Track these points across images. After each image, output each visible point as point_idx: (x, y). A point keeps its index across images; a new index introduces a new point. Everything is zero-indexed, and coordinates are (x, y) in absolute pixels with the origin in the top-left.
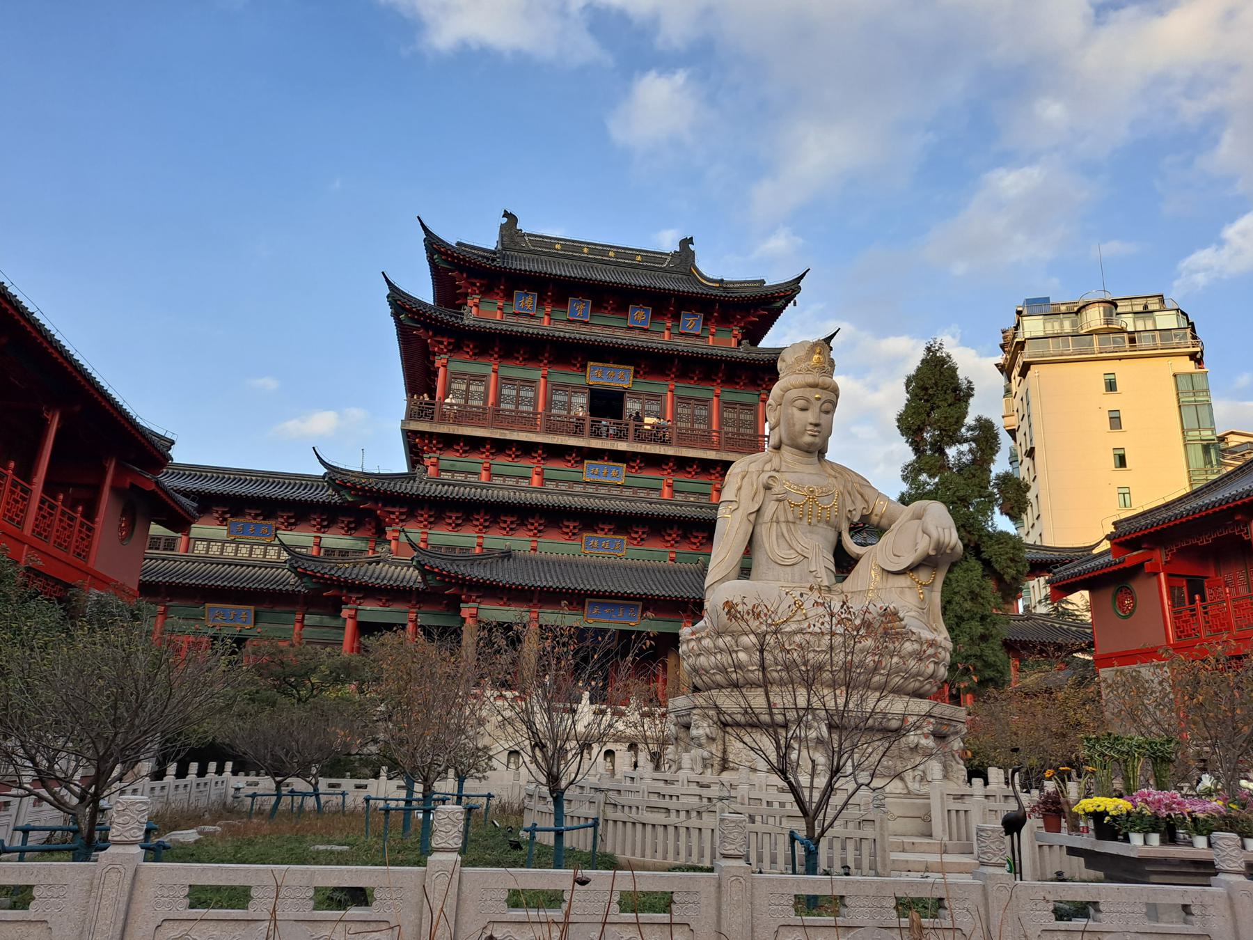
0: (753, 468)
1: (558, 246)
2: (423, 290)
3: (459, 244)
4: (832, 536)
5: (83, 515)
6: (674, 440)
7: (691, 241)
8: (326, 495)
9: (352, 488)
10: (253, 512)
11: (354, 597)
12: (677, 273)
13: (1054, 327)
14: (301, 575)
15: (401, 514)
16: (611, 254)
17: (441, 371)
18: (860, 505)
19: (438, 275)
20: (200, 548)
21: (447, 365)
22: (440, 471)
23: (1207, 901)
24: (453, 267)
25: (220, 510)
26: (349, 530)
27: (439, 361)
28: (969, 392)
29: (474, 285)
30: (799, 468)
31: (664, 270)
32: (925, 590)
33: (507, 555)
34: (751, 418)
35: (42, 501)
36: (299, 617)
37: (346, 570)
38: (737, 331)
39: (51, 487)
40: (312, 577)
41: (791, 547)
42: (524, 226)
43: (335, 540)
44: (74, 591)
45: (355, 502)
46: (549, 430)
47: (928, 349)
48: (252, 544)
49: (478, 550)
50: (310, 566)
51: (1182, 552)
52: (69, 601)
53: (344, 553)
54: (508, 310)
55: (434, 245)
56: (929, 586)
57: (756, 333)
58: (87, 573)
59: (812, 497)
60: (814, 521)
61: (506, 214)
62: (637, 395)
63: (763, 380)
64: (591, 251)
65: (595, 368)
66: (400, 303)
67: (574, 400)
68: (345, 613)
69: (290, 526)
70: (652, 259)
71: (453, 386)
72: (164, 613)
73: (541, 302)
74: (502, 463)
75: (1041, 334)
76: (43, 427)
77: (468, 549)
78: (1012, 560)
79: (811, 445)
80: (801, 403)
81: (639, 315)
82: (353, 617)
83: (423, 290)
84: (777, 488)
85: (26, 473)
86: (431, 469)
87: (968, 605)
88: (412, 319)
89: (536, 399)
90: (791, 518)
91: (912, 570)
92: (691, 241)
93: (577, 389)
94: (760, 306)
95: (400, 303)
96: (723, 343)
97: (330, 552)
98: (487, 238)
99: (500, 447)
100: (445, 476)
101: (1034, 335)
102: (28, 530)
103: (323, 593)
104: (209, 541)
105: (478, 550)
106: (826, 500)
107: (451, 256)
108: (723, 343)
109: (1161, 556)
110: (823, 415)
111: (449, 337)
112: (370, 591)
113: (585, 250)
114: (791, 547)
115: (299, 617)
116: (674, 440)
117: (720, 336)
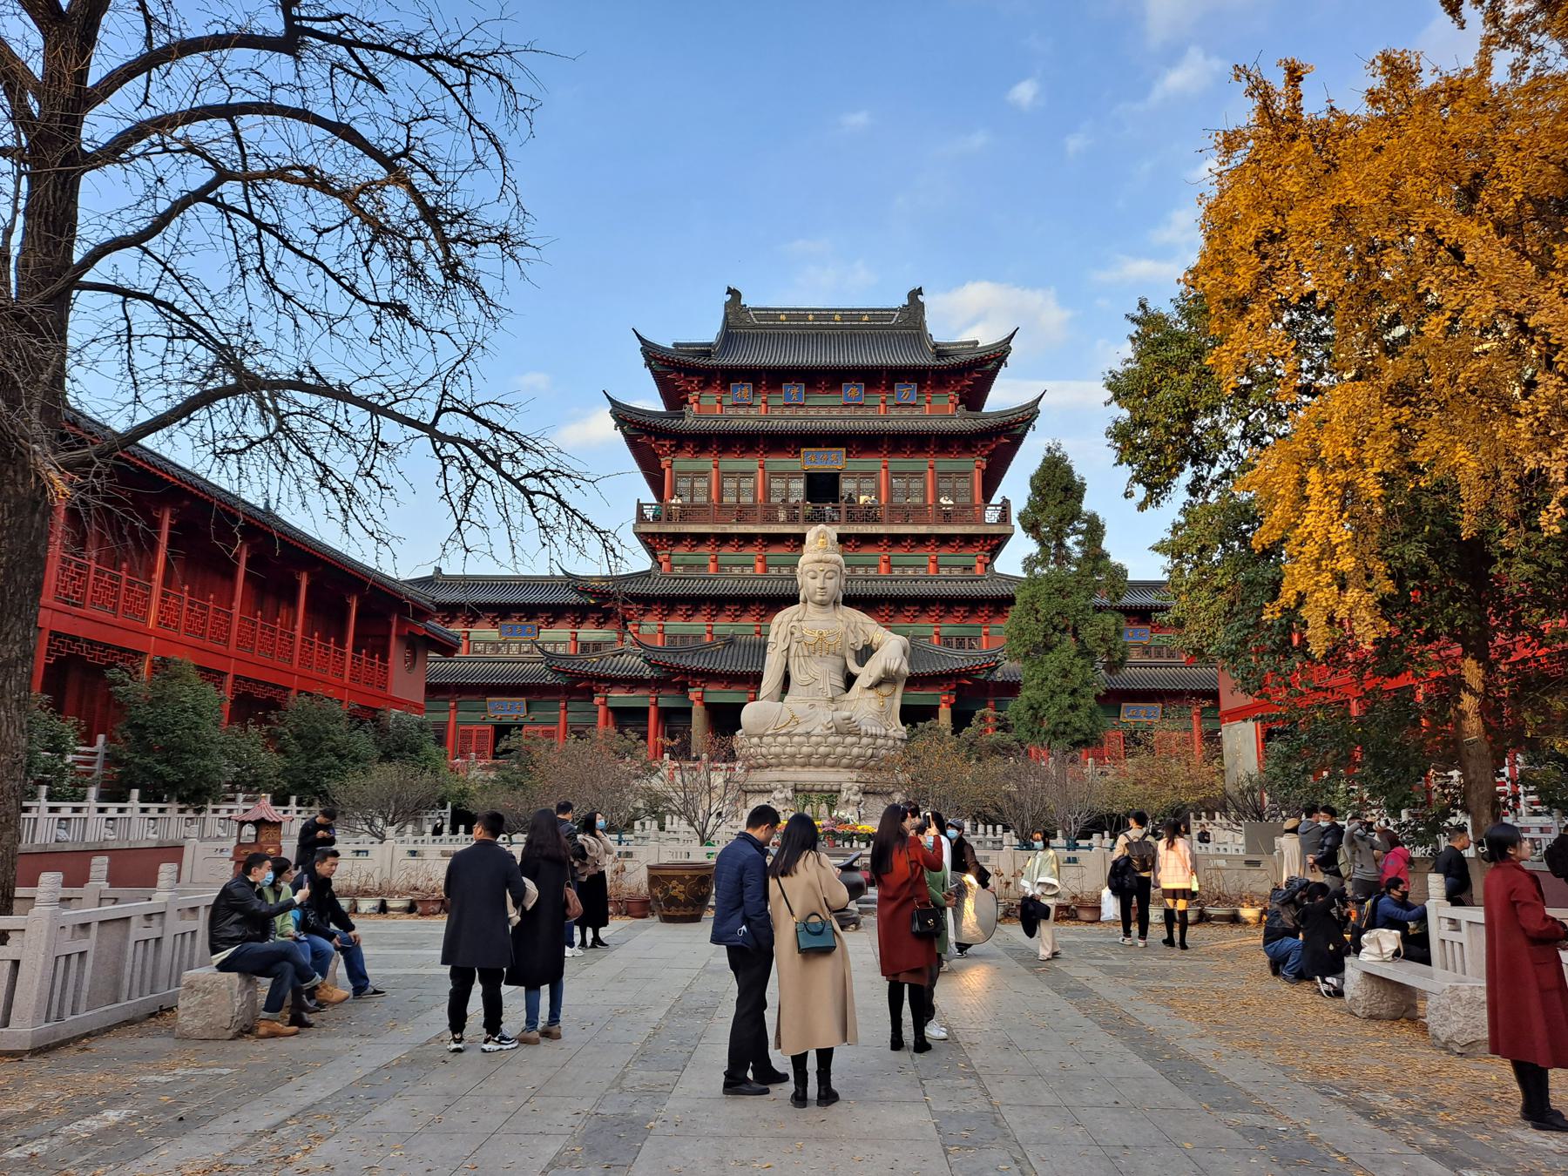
0: (786, 619)
2: (650, 400)
3: (676, 345)
4: (839, 662)
6: (886, 518)
7: (920, 291)
8: (573, 598)
9: (593, 593)
11: (602, 686)
14: (556, 672)
18: (862, 638)
21: (679, 463)
22: (672, 566)
24: (676, 370)
26: (599, 625)
27: (665, 462)
31: (892, 327)
33: (730, 642)
35: (164, 594)
37: (593, 664)
38: (953, 396)
39: (357, 649)
42: (748, 301)
43: (589, 633)
45: (598, 602)
47: (1049, 450)
49: (707, 639)
50: (564, 665)
53: (597, 646)
54: (728, 401)
55: (652, 354)
57: (974, 399)
59: (821, 638)
62: (851, 475)
64: (817, 318)
66: (625, 417)
67: (792, 486)
68: (597, 700)
69: (549, 625)
73: (756, 389)
76: (348, 607)
77: (700, 636)
78: (1103, 640)
81: (853, 391)
82: (605, 704)
83: (650, 400)
85: (341, 643)
92: (920, 291)
93: (793, 475)
94: (973, 372)
96: (939, 412)
97: (585, 646)
98: (707, 330)
100: (679, 570)
102: (347, 680)
103: (577, 685)
105: (707, 639)
108: (939, 412)
112: (615, 682)
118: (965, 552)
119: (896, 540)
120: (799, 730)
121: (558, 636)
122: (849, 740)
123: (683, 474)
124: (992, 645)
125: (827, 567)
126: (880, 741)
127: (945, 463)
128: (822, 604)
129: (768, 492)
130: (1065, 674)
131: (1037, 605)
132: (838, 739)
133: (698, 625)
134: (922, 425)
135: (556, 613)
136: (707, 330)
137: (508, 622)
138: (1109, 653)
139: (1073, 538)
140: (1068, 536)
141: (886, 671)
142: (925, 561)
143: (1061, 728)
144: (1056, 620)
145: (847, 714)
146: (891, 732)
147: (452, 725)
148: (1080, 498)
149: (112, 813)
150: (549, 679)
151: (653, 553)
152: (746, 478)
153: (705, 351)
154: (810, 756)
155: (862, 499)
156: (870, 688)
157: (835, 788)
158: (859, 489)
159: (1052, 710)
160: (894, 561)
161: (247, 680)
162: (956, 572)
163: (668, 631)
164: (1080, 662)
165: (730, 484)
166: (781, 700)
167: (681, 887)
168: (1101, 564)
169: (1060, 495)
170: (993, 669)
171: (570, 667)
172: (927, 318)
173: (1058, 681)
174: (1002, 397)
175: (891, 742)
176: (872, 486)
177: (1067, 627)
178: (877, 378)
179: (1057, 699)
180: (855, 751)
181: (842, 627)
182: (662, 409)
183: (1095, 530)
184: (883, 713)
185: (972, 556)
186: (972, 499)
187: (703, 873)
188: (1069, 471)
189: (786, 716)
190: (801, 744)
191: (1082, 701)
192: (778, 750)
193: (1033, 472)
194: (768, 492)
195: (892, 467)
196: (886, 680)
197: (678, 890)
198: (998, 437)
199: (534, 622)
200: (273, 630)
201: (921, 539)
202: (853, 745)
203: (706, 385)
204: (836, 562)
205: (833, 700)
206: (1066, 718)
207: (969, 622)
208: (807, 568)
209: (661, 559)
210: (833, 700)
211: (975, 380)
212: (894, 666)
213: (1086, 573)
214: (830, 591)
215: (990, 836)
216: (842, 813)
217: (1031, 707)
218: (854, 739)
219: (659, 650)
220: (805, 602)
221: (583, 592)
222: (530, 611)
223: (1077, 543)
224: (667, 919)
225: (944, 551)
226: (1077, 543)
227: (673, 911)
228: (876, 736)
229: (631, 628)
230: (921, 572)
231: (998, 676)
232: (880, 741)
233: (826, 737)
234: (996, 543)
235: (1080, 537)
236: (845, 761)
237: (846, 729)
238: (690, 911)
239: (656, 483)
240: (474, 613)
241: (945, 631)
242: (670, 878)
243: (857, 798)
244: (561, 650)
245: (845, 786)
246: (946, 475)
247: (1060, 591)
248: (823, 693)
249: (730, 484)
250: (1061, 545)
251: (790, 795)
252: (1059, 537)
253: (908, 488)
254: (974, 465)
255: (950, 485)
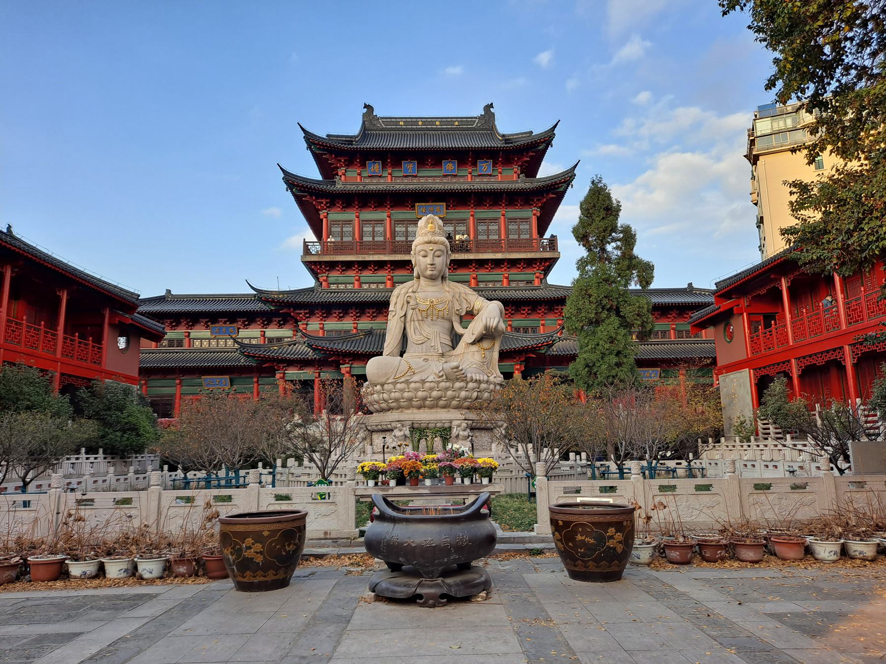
0: (403, 291)
1: (402, 123)
2: (311, 171)
3: (328, 136)
4: (447, 324)
5: (93, 341)
7: (491, 105)
8: (259, 306)
10: (223, 320)
11: (281, 366)
12: (483, 130)
13: (780, 124)
14: (248, 356)
15: (306, 313)
16: (437, 123)
17: (324, 220)
18: (465, 306)
19: (318, 158)
20: (197, 343)
23: (336, 490)
24: (329, 152)
25: (204, 321)
26: (280, 326)
27: (322, 214)
28: (618, 209)
29: (340, 161)
30: (428, 289)
31: (474, 129)
32: (487, 353)
34: (528, 227)
35: (65, 338)
36: (255, 380)
37: (275, 351)
38: (516, 168)
40: (254, 357)
41: (421, 334)
42: (378, 112)
43: (273, 332)
44: (93, 382)
45: (281, 309)
46: (394, 252)
47: (593, 182)
48: (226, 339)
50: (252, 351)
51: (758, 298)
52: (92, 387)
53: (279, 339)
54: (365, 174)
55: (311, 141)
56: (491, 349)
57: (531, 170)
58: (102, 371)
59: (432, 306)
60: (435, 318)
61: (366, 106)
63: (533, 200)
65: (420, 207)
66: (294, 183)
68: (278, 376)
69: (246, 326)
70: (464, 125)
71: (333, 229)
72: (180, 384)
73: (384, 166)
74: (367, 275)
75: (769, 131)
76: (59, 300)
78: (638, 315)
79: (432, 275)
80: (422, 253)
81: (449, 166)
82: (283, 378)
83: (311, 171)
84: (412, 302)
85: (52, 324)
86: (324, 283)
87: (607, 346)
88: (300, 191)
89: (385, 231)
90: (420, 318)
91: (478, 342)
92: (491, 105)
94: (530, 151)
95: (294, 183)
96: (509, 178)
97: (271, 340)
98: (352, 128)
99: (364, 265)
100: (333, 287)
101: (764, 132)
102: (59, 356)
103: (264, 366)
104: (201, 339)
106: (441, 306)
107: (322, 145)
108: (509, 178)
109: (744, 302)
110: (436, 259)
111: (326, 199)
113: (420, 123)
114: (421, 334)
115: (255, 380)
116: (474, 249)
117: (505, 173)
118: (528, 271)
119: (481, 263)
120: (416, 378)
121: (251, 334)
122: (458, 385)
123: (335, 222)
124: (545, 329)
125: (435, 247)
126: (483, 386)
127: (512, 213)
128: (432, 278)
129: (393, 234)
130: (612, 340)
131: (590, 292)
132: (448, 384)
133: (347, 324)
134: (496, 186)
135: (250, 318)
136: (354, 129)
137: (217, 325)
138: (642, 326)
139: (613, 244)
140: (609, 243)
141: (486, 328)
142: (500, 278)
143: (610, 380)
144: (605, 301)
145: (455, 364)
146: (492, 378)
147: (178, 395)
148: (617, 216)
149: (92, 460)
150: (243, 361)
151: (315, 274)
152: (375, 224)
153: (349, 140)
154: (425, 399)
155: (458, 237)
156: (473, 343)
157: (447, 425)
158: (455, 231)
159: (604, 367)
160: (480, 278)
161: (70, 376)
162: (522, 285)
163: (327, 327)
164: (623, 331)
165: (367, 229)
166: (401, 355)
167: (258, 547)
168: (634, 262)
169: (603, 213)
170: (550, 346)
171: (258, 353)
172: (496, 123)
173: (607, 346)
174: (548, 169)
175: (492, 387)
176: (464, 228)
177: (611, 308)
178: (466, 157)
179: (606, 359)
180: (463, 394)
181: (449, 297)
182: (320, 178)
183: (629, 238)
184: (485, 363)
185: (532, 274)
186: (531, 235)
187: (289, 526)
188: (608, 196)
189: (404, 367)
190: (417, 390)
191: (625, 360)
192: (397, 395)
193: (582, 199)
194: (393, 234)
195: (478, 216)
196: (488, 335)
197: (253, 551)
198: (547, 194)
199: (235, 325)
200: (72, 340)
201: (497, 263)
202: (461, 389)
203: (349, 164)
204: (443, 243)
205: (443, 355)
206: (613, 373)
207: (532, 317)
208: (419, 248)
209: (321, 280)
210: (443, 355)
211: (531, 157)
212: (493, 323)
213: (625, 268)
214: (439, 267)
215: (578, 462)
216: (456, 446)
217: (587, 366)
218: (462, 384)
219: (319, 339)
220: (418, 278)
221: (266, 301)
222: (232, 317)
223: (617, 248)
224: (243, 587)
225: (513, 271)
226: (617, 248)
227: (248, 578)
228: (479, 382)
229: (301, 327)
230: (498, 285)
231: (556, 349)
232: (483, 386)
233: (438, 382)
234: (548, 264)
235: (619, 243)
236: (454, 403)
237: (456, 375)
238: (271, 577)
239: (317, 230)
240: (193, 319)
241: (515, 324)
242: (243, 536)
243: (466, 433)
244: (254, 342)
245: (455, 423)
246: (513, 220)
247: (606, 280)
248: (434, 341)
249: (367, 229)
250: (603, 250)
251: (408, 433)
252: (603, 242)
253: (488, 230)
254: (531, 213)
255: (516, 227)
